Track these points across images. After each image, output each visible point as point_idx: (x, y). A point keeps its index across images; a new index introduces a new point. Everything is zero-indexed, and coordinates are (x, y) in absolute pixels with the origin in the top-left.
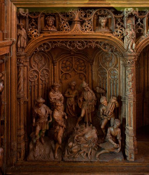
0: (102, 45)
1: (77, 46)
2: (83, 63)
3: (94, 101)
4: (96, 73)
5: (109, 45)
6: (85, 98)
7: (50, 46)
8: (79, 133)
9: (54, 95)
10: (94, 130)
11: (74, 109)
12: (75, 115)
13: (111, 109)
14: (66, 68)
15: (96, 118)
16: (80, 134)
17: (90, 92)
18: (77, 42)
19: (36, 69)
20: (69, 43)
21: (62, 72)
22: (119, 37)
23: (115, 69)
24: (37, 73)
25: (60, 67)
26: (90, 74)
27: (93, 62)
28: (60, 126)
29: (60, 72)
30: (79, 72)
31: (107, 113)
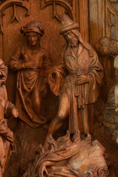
3: (97, 71)
6: (68, 65)
8: (54, 155)
10: (98, 147)
11: (38, 100)
12: (42, 120)
15: (103, 124)
16: (57, 158)
17: (84, 47)
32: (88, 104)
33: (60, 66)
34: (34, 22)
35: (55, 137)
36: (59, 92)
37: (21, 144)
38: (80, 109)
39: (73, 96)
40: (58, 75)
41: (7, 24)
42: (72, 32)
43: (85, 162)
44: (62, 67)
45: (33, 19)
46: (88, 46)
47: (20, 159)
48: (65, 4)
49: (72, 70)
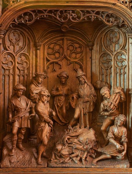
0: (104, 17)
1: (71, 17)
2: (79, 47)
3: (93, 96)
4: (97, 62)
5: (113, 17)
6: (80, 93)
7: (34, 17)
9: (37, 88)
11: (64, 111)
12: (67, 121)
13: (114, 101)
14: (54, 54)
15: (97, 124)
17: (87, 84)
18: (71, 12)
19: (11, 52)
20: (59, 14)
21: (48, 60)
22: (126, 5)
23: (123, 51)
24: (13, 57)
25: (46, 54)
26: (89, 63)
27: (93, 45)
28: (45, 122)
29: (45, 60)
30: (73, 60)
31: (109, 105)
32: (89, 112)
33: (76, 94)
34: (64, 72)
35: (72, 127)
36: (75, 107)
37: (55, 133)
38: (85, 114)
39: (82, 108)
40: (75, 98)
41: (50, 73)
42: (82, 77)
43: (86, 137)
44: (77, 94)
45: (63, 70)
46: (89, 84)
47: (55, 138)
48: (80, 63)
49: (82, 96)
